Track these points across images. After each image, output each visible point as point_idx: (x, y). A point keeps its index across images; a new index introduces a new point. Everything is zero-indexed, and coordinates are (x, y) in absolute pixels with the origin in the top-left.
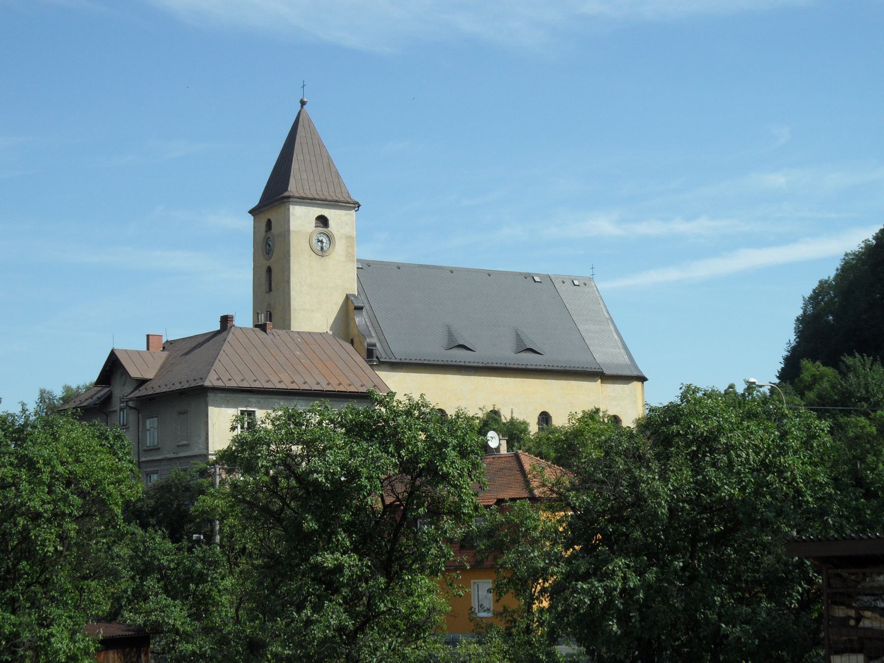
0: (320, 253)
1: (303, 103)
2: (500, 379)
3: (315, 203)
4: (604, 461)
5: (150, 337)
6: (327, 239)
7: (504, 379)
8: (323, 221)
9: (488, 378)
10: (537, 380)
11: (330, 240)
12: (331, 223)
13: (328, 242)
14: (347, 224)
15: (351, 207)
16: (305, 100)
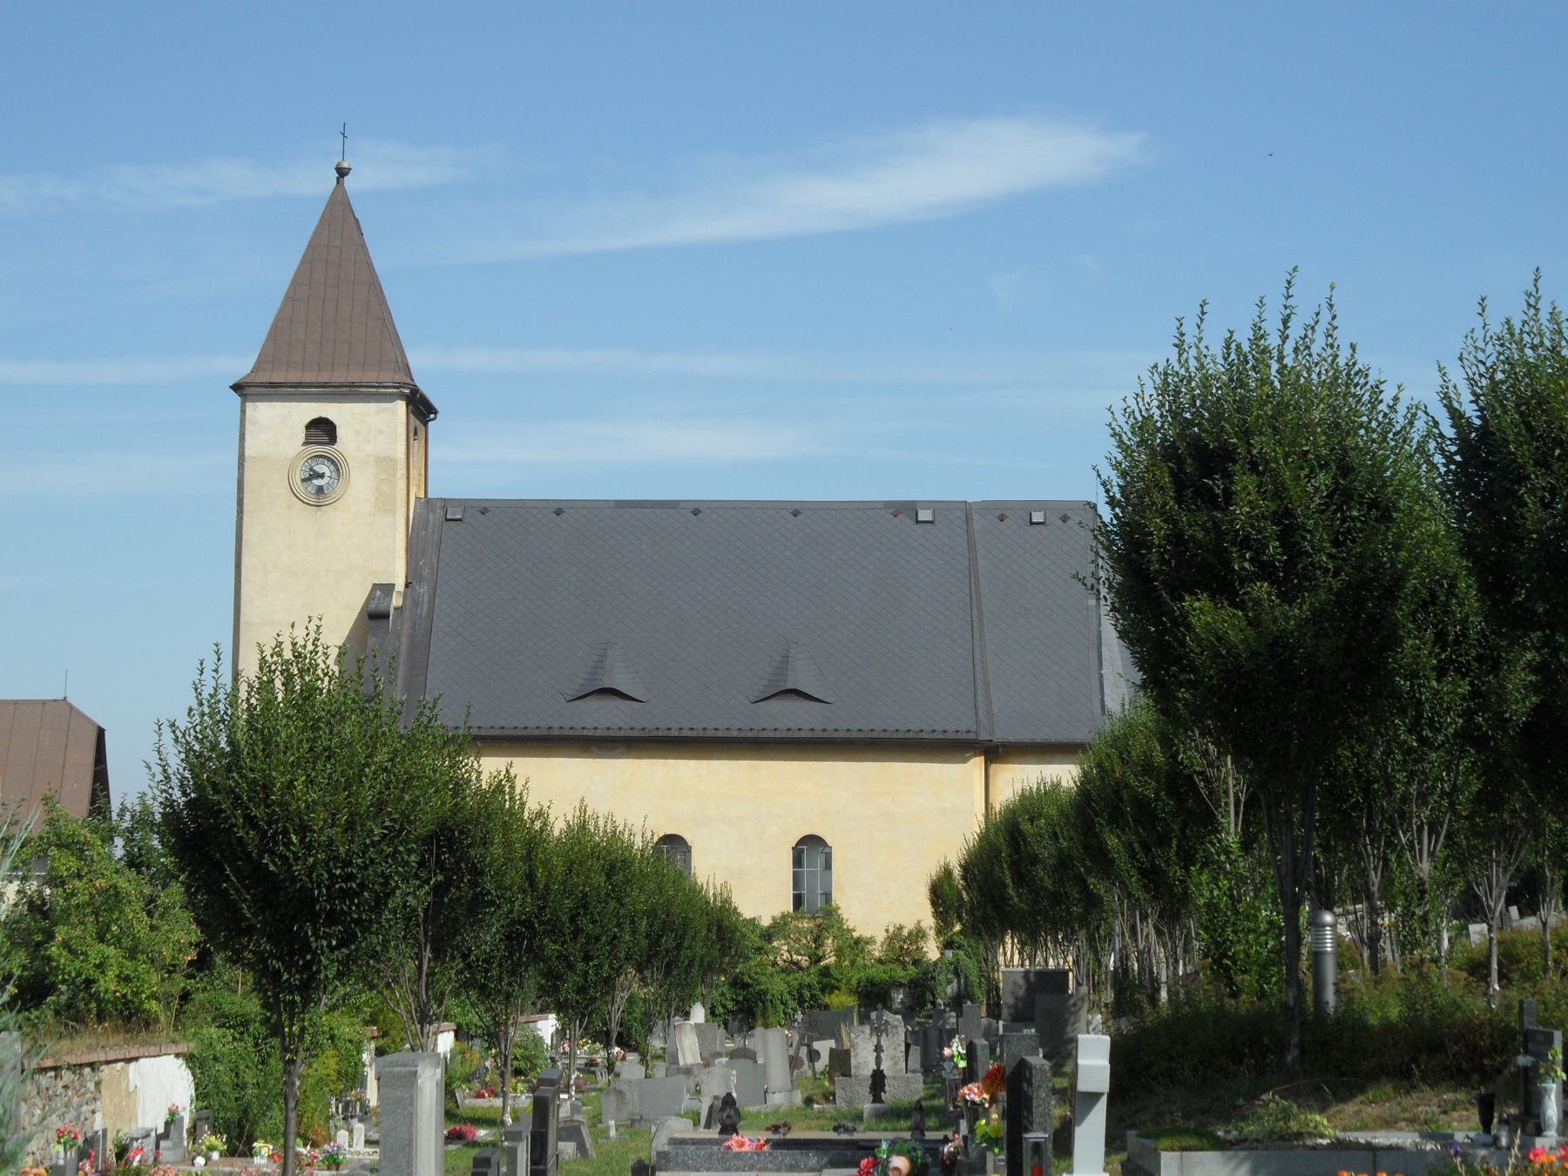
0: (313, 500)
1: (342, 172)
2: (693, 763)
3: (303, 394)
4: (1258, 409)
5: (449, 517)
6: (332, 467)
7: (704, 763)
8: (323, 430)
9: (661, 762)
10: (796, 763)
11: (338, 470)
12: (339, 432)
13: (334, 475)
14: (381, 432)
15: (391, 394)
16: (345, 165)
